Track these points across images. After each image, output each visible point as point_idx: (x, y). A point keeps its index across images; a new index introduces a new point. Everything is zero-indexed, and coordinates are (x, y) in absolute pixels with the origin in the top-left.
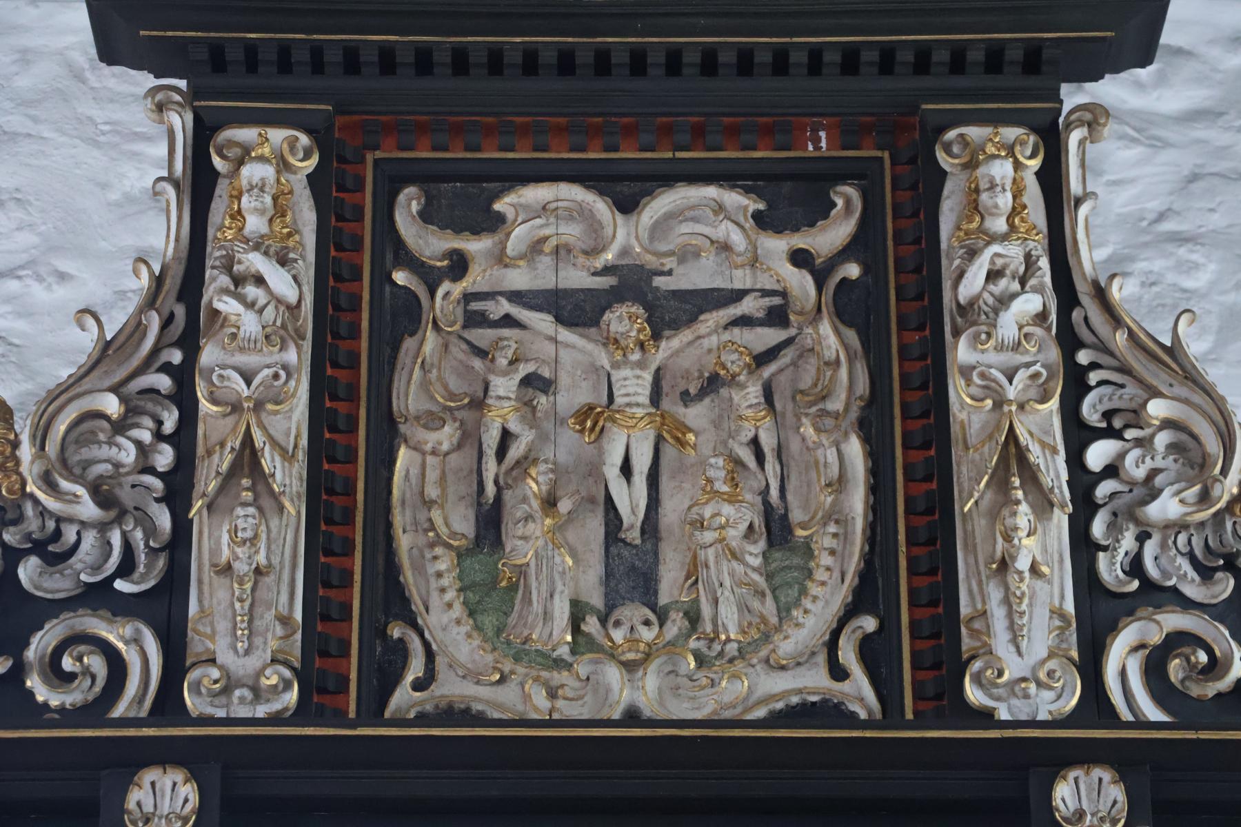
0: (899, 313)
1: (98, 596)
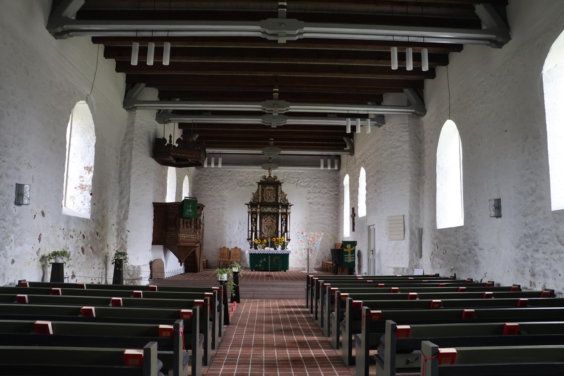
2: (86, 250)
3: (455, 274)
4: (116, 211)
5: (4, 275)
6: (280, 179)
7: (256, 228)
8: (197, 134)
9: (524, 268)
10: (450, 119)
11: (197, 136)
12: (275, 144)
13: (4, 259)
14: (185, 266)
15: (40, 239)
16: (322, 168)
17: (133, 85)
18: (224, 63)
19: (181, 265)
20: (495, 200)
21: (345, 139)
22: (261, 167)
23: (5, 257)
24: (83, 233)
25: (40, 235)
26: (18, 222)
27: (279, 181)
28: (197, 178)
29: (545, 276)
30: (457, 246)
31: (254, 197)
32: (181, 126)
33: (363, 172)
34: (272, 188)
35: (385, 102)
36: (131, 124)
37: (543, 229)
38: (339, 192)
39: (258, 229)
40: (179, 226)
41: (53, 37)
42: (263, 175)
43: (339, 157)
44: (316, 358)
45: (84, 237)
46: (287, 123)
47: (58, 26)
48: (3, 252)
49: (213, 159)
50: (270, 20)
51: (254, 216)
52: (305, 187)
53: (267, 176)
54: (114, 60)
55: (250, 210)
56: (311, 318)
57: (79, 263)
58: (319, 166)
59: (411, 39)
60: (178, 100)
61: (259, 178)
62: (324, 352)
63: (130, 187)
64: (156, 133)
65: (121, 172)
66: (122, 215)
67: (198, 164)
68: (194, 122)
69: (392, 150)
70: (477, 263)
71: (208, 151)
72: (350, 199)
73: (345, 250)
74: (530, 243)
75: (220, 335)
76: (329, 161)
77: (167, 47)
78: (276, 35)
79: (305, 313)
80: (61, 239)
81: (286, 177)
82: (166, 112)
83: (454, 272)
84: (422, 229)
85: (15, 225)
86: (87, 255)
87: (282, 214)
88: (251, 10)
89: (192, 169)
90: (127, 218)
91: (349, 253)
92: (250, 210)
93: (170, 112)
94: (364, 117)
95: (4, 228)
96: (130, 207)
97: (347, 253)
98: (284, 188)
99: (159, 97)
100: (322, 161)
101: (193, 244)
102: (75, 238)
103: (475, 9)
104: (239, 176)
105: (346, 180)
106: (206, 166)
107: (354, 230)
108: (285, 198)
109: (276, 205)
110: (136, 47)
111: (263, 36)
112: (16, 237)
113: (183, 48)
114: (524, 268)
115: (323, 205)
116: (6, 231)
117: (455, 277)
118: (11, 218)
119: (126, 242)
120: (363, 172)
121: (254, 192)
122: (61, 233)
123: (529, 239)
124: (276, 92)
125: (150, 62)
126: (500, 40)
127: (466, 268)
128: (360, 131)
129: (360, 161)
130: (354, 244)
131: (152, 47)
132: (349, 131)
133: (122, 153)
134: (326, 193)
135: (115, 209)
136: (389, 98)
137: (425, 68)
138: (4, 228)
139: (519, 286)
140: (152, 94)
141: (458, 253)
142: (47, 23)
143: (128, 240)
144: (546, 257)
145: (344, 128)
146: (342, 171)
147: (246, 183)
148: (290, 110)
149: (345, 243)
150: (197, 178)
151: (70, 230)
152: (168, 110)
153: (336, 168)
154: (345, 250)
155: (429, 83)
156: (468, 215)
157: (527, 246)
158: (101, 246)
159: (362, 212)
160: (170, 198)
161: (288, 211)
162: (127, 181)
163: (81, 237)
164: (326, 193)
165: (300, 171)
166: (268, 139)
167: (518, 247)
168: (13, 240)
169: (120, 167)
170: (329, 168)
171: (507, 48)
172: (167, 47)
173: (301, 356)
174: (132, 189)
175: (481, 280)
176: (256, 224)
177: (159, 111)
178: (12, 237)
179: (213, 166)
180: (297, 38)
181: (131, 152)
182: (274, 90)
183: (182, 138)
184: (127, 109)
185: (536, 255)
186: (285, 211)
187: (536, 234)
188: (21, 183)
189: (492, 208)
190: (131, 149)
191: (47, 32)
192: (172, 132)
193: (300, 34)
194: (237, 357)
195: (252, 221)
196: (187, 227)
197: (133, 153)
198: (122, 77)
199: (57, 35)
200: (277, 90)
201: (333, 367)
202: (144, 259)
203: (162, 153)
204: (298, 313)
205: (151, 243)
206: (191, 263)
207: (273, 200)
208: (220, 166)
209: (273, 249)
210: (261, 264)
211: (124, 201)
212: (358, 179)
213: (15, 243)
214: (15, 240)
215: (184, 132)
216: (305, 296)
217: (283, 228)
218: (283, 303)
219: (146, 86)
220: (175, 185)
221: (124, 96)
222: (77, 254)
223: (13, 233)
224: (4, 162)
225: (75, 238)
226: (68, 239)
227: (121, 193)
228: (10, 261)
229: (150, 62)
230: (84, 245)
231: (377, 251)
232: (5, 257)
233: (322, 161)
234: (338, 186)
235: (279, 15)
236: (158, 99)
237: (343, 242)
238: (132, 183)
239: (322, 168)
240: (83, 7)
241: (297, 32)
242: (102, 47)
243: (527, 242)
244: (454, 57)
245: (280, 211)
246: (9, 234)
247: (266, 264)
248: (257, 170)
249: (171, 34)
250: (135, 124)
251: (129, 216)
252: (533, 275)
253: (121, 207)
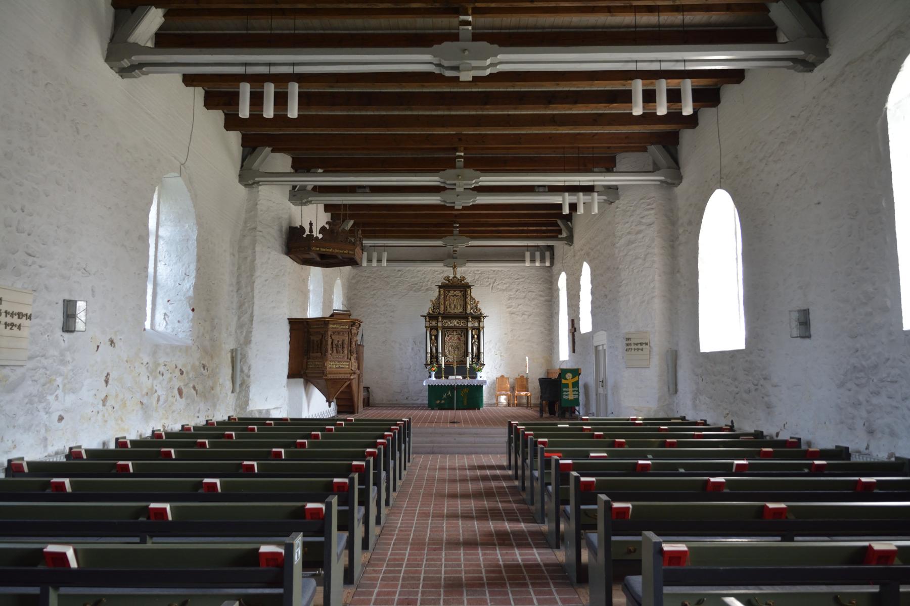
0: (465, 296)
2: (185, 391)
3: (732, 422)
4: (233, 332)
5: (46, 439)
6: (469, 280)
7: (437, 349)
8: (350, 219)
9: (853, 419)
10: (721, 188)
11: (352, 222)
12: (460, 232)
13: (46, 416)
14: (338, 405)
15: (107, 382)
16: (527, 264)
17: (254, 149)
18: (384, 116)
19: (330, 406)
20: (799, 311)
21: (559, 222)
22: (442, 264)
23: (47, 413)
24: (180, 367)
25: (108, 374)
26: (69, 358)
27: (467, 284)
28: (354, 281)
29: (893, 434)
30: (735, 379)
32: (327, 208)
33: (586, 269)
34: (458, 293)
35: (619, 167)
36: (253, 207)
37: (888, 359)
38: (552, 296)
39: (440, 350)
40: (326, 351)
41: (117, 75)
42: (445, 274)
43: (551, 248)
44: (526, 566)
45: (182, 373)
46: (477, 202)
47: (121, 55)
48: (44, 404)
49: (375, 256)
50: (446, 45)
51: (434, 332)
52: (504, 290)
53: (451, 276)
54: (221, 112)
55: (428, 325)
56: (515, 487)
57: (173, 412)
58: (524, 261)
59: (666, 66)
60: (320, 171)
61: (440, 279)
62: (537, 555)
63: (253, 297)
64: (290, 219)
65: (239, 276)
66: (242, 339)
67: (352, 262)
68: (345, 202)
69: (629, 237)
70: (769, 406)
71: (367, 243)
72: (569, 306)
73: (564, 381)
74: (863, 381)
75: (378, 522)
76: (538, 254)
77: (294, 89)
78: (456, 68)
79: (506, 478)
80: (144, 379)
81: (477, 277)
82: (303, 188)
83: (730, 418)
84: (676, 351)
85: (63, 362)
86: (187, 399)
87: (473, 329)
88: (418, 32)
89: (347, 269)
90: (250, 342)
91: (570, 386)
92: (428, 325)
93: (310, 188)
94: (588, 189)
95: (45, 368)
96: (254, 325)
97: (567, 386)
98: (475, 293)
99: (292, 167)
100: (528, 254)
101: (347, 376)
102: (167, 376)
103: (769, 11)
105: (562, 281)
106: (365, 264)
107: (574, 351)
108: (476, 307)
109: (464, 317)
110: (245, 90)
111: (437, 71)
112: (66, 381)
113: (318, 91)
114: (853, 419)
115: (530, 315)
116: (48, 372)
117: (731, 428)
118: (56, 353)
119: (249, 376)
120: (586, 269)
121: (434, 299)
122: (143, 370)
123: (862, 374)
124: (460, 157)
125: (269, 112)
126: (811, 58)
127: (751, 413)
128: (582, 211)
129: (582, 253)
130: (576, 372)
131: (270, 90)
132: (566, 211)
133: (241, 249)
134: (533, 299)
135: (233, 328)
136: (624, 160)
137: (688, 110)
138: (45, 368)
139: (847, 448)
140: (282, 162)
141: (736, 390)
142: (105, 53)
143: (251, 373)
144: (894, 404)
145: (559, 206)
146: (556, 268)
148: (480, 184)
149: (563, 372)
150: (354, 281)
151: (159, 364)
152: (306, 186)
153: (548, 264)
154: (564, 381)
155: (687, 136)
156: (753, 334)
157: (858, 385)
158: (210, 383)
159: (586, 325)
160: (313, 312)
161: (481, 324)
162: (249, 289)
163: (178, 373)
164: (533, 299)
165: (497, 269)
166: (451, 225)
167: (842, 385)
168: (61, 386)
169: (239, 268)
170: (538, 264)
171: (820, 71)
172: (294, 89)
173: (501, 563)
174: (256, 300)
175: (777, 434)
176: (437, 343)
177: (294, 187)
178: (59, 380)
179: (375, 264)
180: (488, 72)
181: (254, 249)
182: (458, 154)
183: (327, 226)
184: (246, 185)
185: (875, 400)
186: (476, 324)
187: (876, 366)
188: (72, 299)
189: (794, 324)
190: (254, 243)
191: (107, 66)
192: (313, 217)
193: (493, 65)
194: (401, 566)
195: (431, 339)
196: (338, 352)
197: (258, 249)
198: (234, 138)
199: (124, 72)
200: (462, 154)
201: (552, 586)
202: (279, 397)
203: (297, 245)
204: (496, 478)
205: (286, 376)
206: (344, 399)
207: (459, 310)
208: (384, 263)
209: (461, 377)
210: (445, 399)
211: (246, 318)
212: (579, 280)
213: (64, 391)
214: (64, 385)
215: (332, 215)
216: (505, 448)
217: (475, 348)
218: (475, 460)
219: (273, 151)
220: (320, 293)
221: (239, 166)
222: (170, 399)
223: (61, 375)
224: (41, 267)
225: (167, 376)
226: (155, 378)
227: (241, 306)
228: (56, 418)
229: (269, 112)
230: (182, 384)
231: (610, 382)
232: (47, 413)
233: (528, 254)
234: (550, 289)
235: (461, 37)
236: (292, 171)
237: (562, 370)
238: (256, 292)
239: (527, 264)
240: (161, 28)
241: (488, 62)
242: (198, 94)
243: (857, 378)
244: (729, 92)
245: (470, 325)
246: (53, 377)
247: (451, 399)
248: (436, 268)
249: (299, 70)
250: (258, 206)
251: (253, 339)
252: (871, 432)
253: (240, 326)
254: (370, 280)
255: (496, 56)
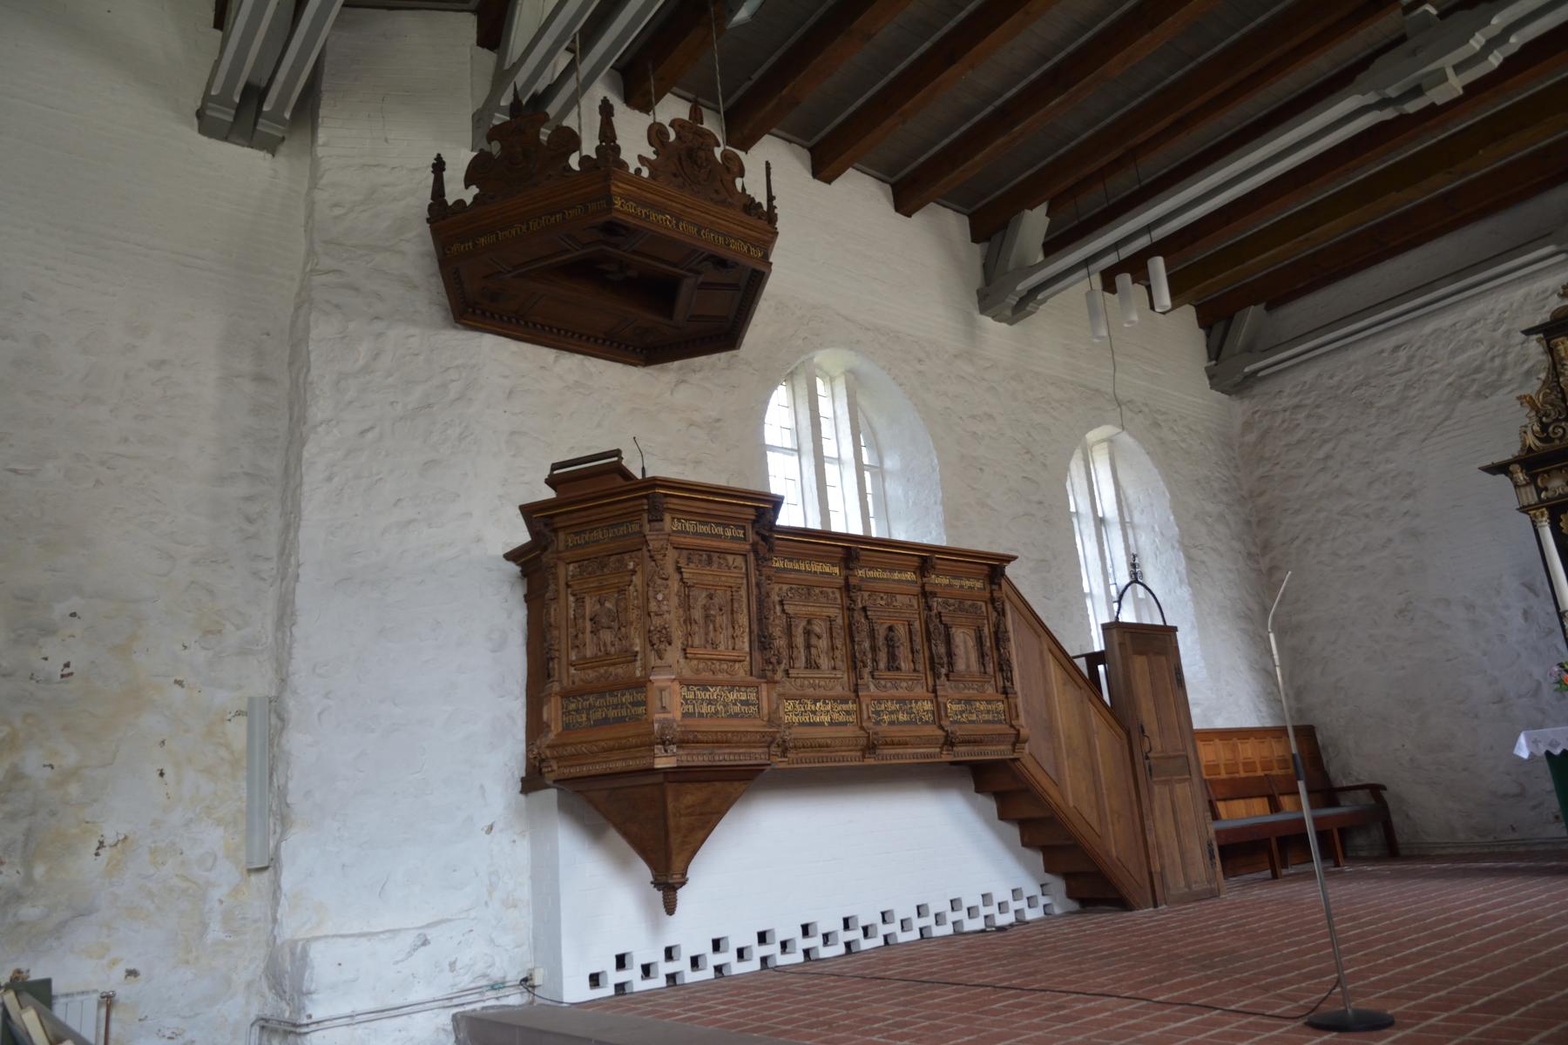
1: (1557, 420)
28: (1251, 437)
31: (1539, 413)
55: (1530, 496)
92: (1530, 496)
104: (1453, 353)
111: (1388, 114)
147: (1504, 369)
150: (1251, 437)
254: (1301, 416)
255: (1488, 23)
